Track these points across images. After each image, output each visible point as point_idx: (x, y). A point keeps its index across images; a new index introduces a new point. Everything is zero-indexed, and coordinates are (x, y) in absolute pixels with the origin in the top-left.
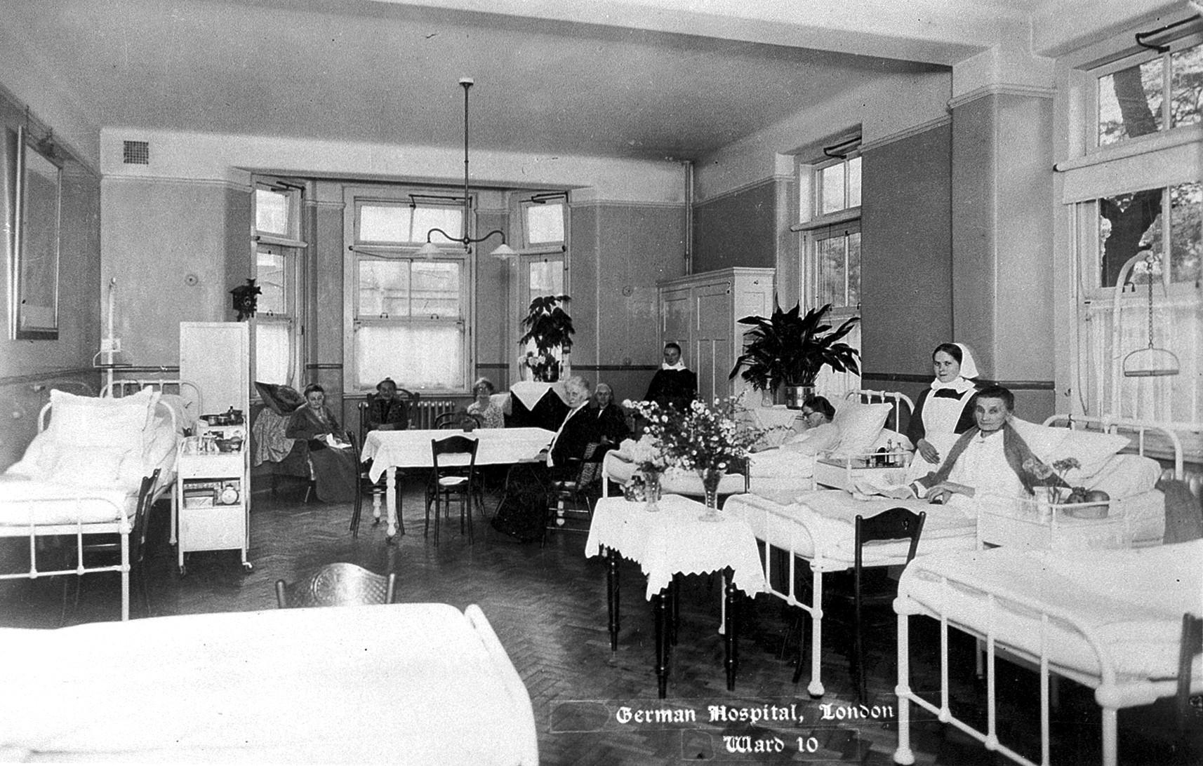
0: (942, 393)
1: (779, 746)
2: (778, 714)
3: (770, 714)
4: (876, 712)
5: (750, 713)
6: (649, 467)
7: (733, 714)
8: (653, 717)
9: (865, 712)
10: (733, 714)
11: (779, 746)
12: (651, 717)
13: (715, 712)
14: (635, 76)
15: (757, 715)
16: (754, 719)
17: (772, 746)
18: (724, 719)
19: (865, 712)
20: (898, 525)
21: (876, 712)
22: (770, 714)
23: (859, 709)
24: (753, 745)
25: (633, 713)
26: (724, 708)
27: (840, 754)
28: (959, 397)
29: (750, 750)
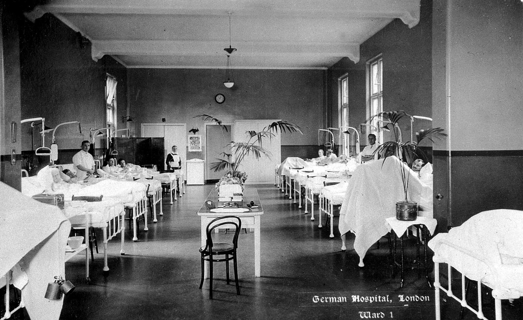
1: (383, 315)
2: (381, 299)
3: (378, 299)
5: (369, 299)
7: (362, 299)
8: (328, 300)
9: (418, 299)
10: (362, 299)
11: (383, 315)
13: (355, 298)
15: (372, 299)
16: (371, 301)
17: (379, 316)
19: (418, 299)
22: (378, 299)
24: (371, 316)
25: (320, 298)
26: (358, 296)
29: (370, 317)
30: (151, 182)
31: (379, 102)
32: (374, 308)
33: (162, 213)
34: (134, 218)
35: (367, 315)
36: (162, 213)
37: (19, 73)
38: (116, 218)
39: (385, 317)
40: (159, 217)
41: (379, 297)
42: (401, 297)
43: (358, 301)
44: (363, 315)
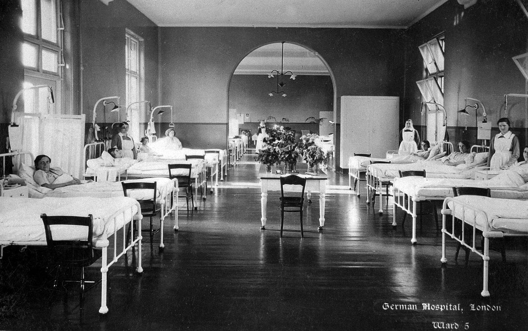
0: (405, 131)
1: (457, 326)
2: (452, 307)
3: (449, 307)
4: (494, 308)
5: (440, 307)
6: (346, 171)
7: (433, 307)
8: (398, 307)
9: (489, 308)
10: (433, 307)
11: (457, 326)
12: (397, 307)
14: (39, 36)
15: (443, 307)
16: (442, 309)
17: (453, 326)
18: (429, 309)
19: (489, 308)
20: (237, 137)
21: (494, 308)
22: (449, 307)
23: (487, 307)
24: (445, 326)
25: (390, 305)
26: (429, 304)
27: (99, 130)
28: (412, 131)
30: (111, 169)
31: (327, 73)
32: (447, 317)
33: (226, 174)
34: (222, 167)
35: (441, 325)
36: (226, 174)
37: (422, 199)
38: (120, 232)
39: (460, 328)
40: (224, 176)
41: (450, 305)
42: (473, 306)
43: (429, 309)
44: (437, 325)
